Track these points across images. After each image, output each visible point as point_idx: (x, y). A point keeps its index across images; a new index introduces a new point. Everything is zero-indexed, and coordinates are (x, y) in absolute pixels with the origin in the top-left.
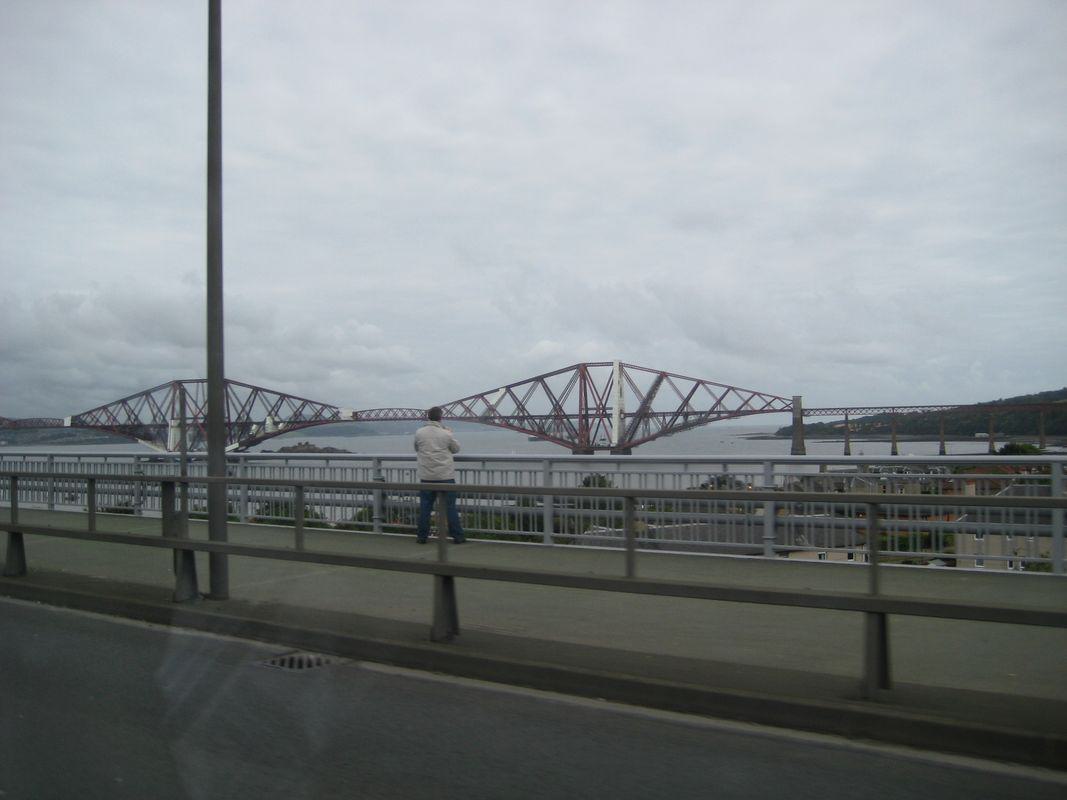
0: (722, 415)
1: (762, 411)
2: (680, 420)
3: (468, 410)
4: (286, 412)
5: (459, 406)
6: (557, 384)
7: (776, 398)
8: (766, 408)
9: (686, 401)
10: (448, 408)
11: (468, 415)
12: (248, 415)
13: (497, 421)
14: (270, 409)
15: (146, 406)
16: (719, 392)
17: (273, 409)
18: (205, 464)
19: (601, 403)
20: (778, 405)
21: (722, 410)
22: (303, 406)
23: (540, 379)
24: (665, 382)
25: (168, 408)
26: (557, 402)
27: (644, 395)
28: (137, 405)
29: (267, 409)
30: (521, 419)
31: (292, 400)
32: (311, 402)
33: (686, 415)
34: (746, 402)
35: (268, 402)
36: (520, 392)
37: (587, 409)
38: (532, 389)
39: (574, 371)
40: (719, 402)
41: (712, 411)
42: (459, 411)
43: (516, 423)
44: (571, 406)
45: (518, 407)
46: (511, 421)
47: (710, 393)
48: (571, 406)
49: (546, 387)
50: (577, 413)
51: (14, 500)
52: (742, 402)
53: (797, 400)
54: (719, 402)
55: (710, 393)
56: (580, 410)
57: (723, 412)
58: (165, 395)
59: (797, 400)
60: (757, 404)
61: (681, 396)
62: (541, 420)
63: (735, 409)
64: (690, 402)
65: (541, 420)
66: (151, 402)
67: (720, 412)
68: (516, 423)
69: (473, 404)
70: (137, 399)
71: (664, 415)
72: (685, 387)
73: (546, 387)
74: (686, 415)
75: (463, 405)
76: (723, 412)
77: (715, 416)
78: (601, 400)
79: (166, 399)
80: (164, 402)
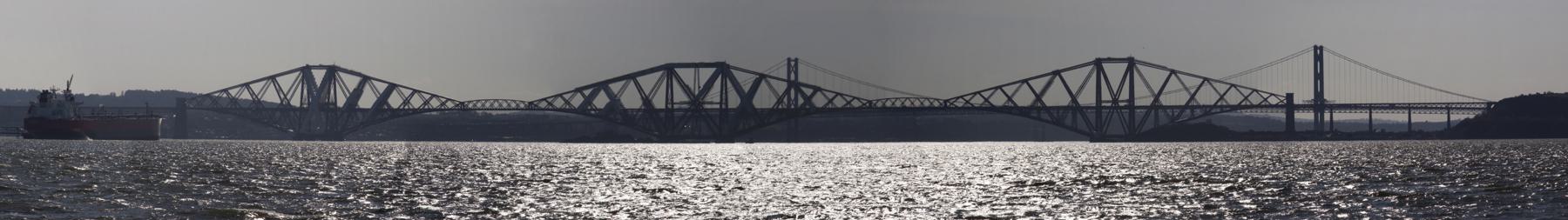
3: (567, 102)
5: (544, 102)
6: (286, 82)
7: (1272, 94)
8: (1243, 103)
9: (1193, 97)
11: (568, 107)
15: (272, 84)
16: (1193, 83)
18: (1284, 110)
19: (286, 98)
20: (1273, 101)
21: (1224, 104)
22: (412, 95)
23: (1026, 81)
24: (763, 84)
25: (298, 85)
27: (1156, 92)
31: (373, 81)
32: (420, 92)
34: (1246, 98)
36: (615, 87)
37: (673, 103)
38: (1049, 84)
39: (659, 74)
41: (1215, 106)
43: (1034, 114)
49: (637, 84)
51: (1370, 116)
53: (1290, 97)
56: (667, 103)
58: (295, 78)
59: (1290, 97)
61: (784, 80)
63: (1213, 103)
67: (1221, 107)
69: (554, 101)
72: (407, 93)
73: (637, 84)
77: (1218, 110)
78: (285, 96)
79: (1469, 97)
80: (289, 91)
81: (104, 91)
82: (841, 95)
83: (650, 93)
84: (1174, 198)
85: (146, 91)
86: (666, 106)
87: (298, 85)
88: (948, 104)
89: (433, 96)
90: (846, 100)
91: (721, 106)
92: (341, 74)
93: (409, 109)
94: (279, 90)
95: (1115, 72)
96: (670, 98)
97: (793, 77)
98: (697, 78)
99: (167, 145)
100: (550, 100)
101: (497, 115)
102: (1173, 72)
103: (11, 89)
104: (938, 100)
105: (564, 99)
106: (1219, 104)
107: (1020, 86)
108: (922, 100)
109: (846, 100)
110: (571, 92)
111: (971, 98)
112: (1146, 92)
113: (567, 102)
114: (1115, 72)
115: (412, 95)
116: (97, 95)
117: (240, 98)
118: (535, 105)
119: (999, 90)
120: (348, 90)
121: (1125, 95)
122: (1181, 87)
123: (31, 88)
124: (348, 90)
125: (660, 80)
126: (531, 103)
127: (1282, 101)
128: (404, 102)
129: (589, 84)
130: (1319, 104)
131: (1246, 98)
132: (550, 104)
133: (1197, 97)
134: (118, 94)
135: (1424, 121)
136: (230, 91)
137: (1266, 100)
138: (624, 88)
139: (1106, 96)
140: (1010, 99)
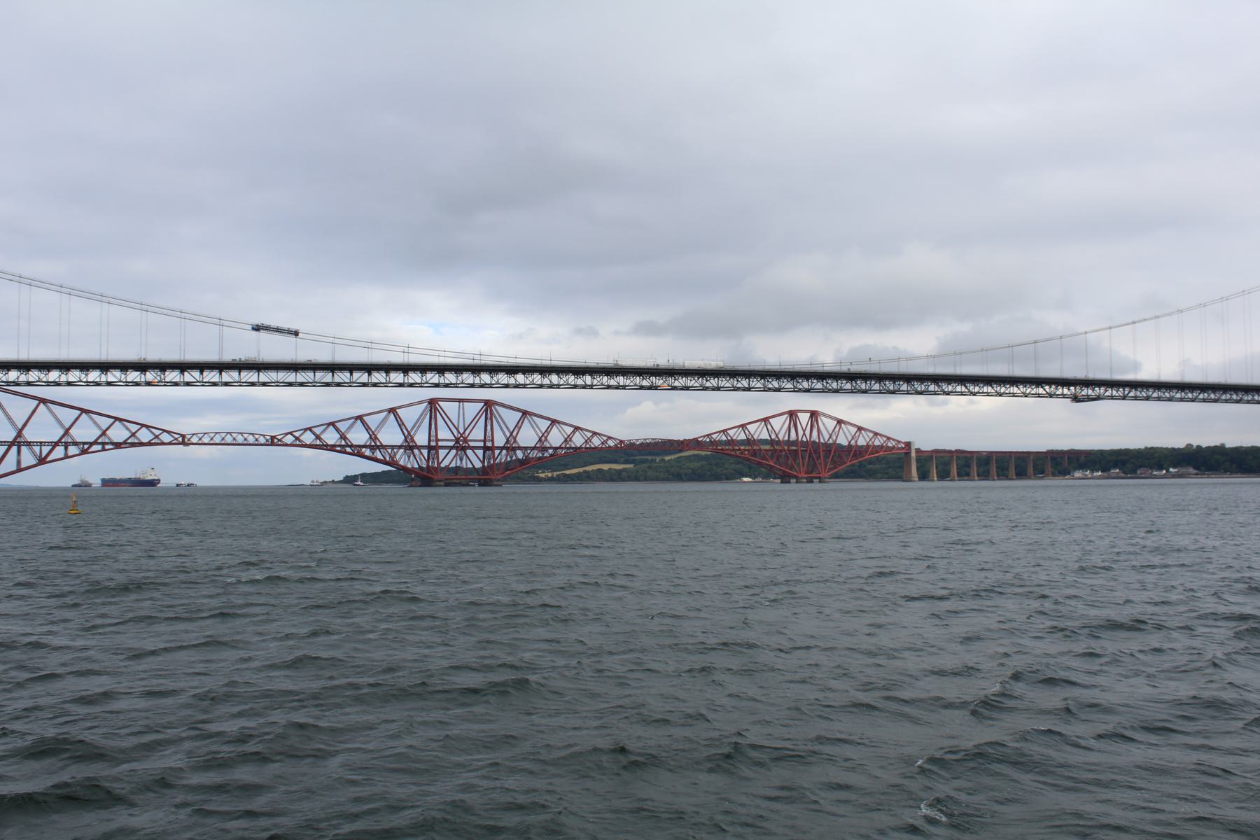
0: (107, 447)
1: (149, 444)
2: (59, 452)
5: (289, 436)
8: (153, 441)
10: (279, 437)
12: (515, 438)
13: (348, 450)
14: (508, 435)
17: (853, 438)
21: (107, 441)
22: (574, 432)
25: (785, 433)
26: (409, 433)
28: (739, 434)
29: (537, 434)
30: (372, 448)
31: (535, 418)
33: (66, 445)
35: (539, 429)
38: (384, 421)
40: (104, 433)
41: (95, 443)
42: (289, 439)
43: (367, 452)
44: (421, 438)
45: (341, 436)
46: (364, 450)
47: (95, 423)
48: (421, 438)
50: (427, 444)
52: (99, 433)
54: (67, 432)
55: (95, 423)
56: (430, 440)
57: (107, 443)
58: (783, 421)
60: (118, 433)
62: (393, 449)
63: (533, 446)
64: (23, 432)
65: (393, 449)
66: (746, 431)
67: (103, 444)
68: (367, 452)
70: (759, 423)
72: (569, 430)
74: (66, 445)
75: (338, 430)
76: (107, 443)
81: (1137, 447)
82: (147, 427)
83: (412, 429)
85: (375, 473)
86: (520, 448)
87: (482, 415)
88: (276, 440)
89: (595, 434)
91: (485, 444)
92: (497, 407)
93: (590, 448)
94: (401, 424)
95: (804, 418)
97: (858, 433)
98: (462, 413)
100: (297, 434)
101: (706, 455)
103: (349, 475)
104: (264, 436)
105: (294, 436)
106: (129, 441)
107: (326, 428)
108: (134, 428)
110: (302, 430)
111: (323, 432)
113: (318, 437)
114: (804, 418)
115: (574, 432)
116: (1241, 447)
117: (739, 439)
118: (279, 440)
119: (331, 427)
120: (507, 428)
124: (507, 428)
126: (273, 438)
127: (176, 439)
128: (566, 440)
129: (28, 424)
130: (41, 446)
131: (133, 435)
132: (297, 438)
133: (24, 432)
134: (1227, 446)
135: (1182, 445)
136: (713, 436)
137: (157, 437)
140: (343, 437)
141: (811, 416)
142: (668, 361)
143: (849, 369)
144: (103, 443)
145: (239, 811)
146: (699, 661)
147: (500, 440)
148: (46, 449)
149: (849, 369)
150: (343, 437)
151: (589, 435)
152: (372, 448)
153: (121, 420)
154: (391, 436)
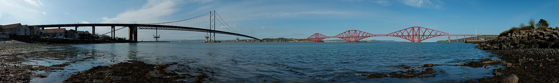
2: (429, 37)
4: (427, 33)
16: (436, 32)
36: (402, 31)
40: (436, 34)
41: (435, 35)
42: (389, 35)
43: (402, 37)
48: (411, 34)
54: (436, 34)
60: (442, 34)
69: (394, 34)
71: (427, 35)
84: (399, 55)
90: (421, 35)
95: (416, 29)
96: (213, 18)
99: (387, 74)
100: (393, 33)
102: (427, 29)
108: (441, 33)
109: (421, 35)
112: (422, 33)
114: (416, 29)
119: (400, 32)
121: (418, 33)
122: (424, 32)
123: (506, 30)
125: (411, 30)
126: (387, 35)
138: (404, 32)
139: (414, 33)
140: (397, 34)
141: (419, 29)
142: (200, 2)
143: (543, 22)
144: (436, 35)
145: (301, 73)
146: (283, 66)
147: (421, 34)
148: (428, 36)
149: (543, 22)
150: (397, 34)
151: (366, 33)
152: (403, 36)
153: (434, 30)
154: (406, 34)
